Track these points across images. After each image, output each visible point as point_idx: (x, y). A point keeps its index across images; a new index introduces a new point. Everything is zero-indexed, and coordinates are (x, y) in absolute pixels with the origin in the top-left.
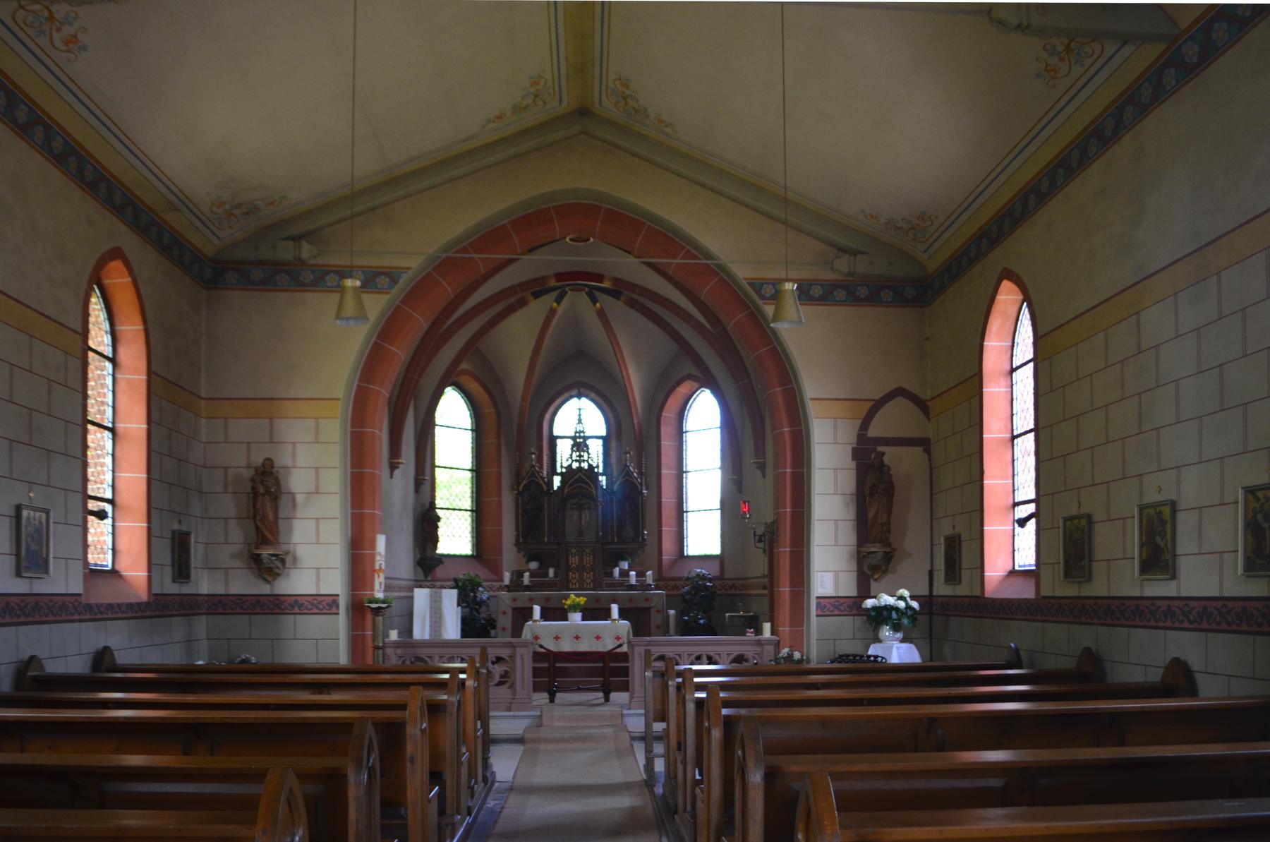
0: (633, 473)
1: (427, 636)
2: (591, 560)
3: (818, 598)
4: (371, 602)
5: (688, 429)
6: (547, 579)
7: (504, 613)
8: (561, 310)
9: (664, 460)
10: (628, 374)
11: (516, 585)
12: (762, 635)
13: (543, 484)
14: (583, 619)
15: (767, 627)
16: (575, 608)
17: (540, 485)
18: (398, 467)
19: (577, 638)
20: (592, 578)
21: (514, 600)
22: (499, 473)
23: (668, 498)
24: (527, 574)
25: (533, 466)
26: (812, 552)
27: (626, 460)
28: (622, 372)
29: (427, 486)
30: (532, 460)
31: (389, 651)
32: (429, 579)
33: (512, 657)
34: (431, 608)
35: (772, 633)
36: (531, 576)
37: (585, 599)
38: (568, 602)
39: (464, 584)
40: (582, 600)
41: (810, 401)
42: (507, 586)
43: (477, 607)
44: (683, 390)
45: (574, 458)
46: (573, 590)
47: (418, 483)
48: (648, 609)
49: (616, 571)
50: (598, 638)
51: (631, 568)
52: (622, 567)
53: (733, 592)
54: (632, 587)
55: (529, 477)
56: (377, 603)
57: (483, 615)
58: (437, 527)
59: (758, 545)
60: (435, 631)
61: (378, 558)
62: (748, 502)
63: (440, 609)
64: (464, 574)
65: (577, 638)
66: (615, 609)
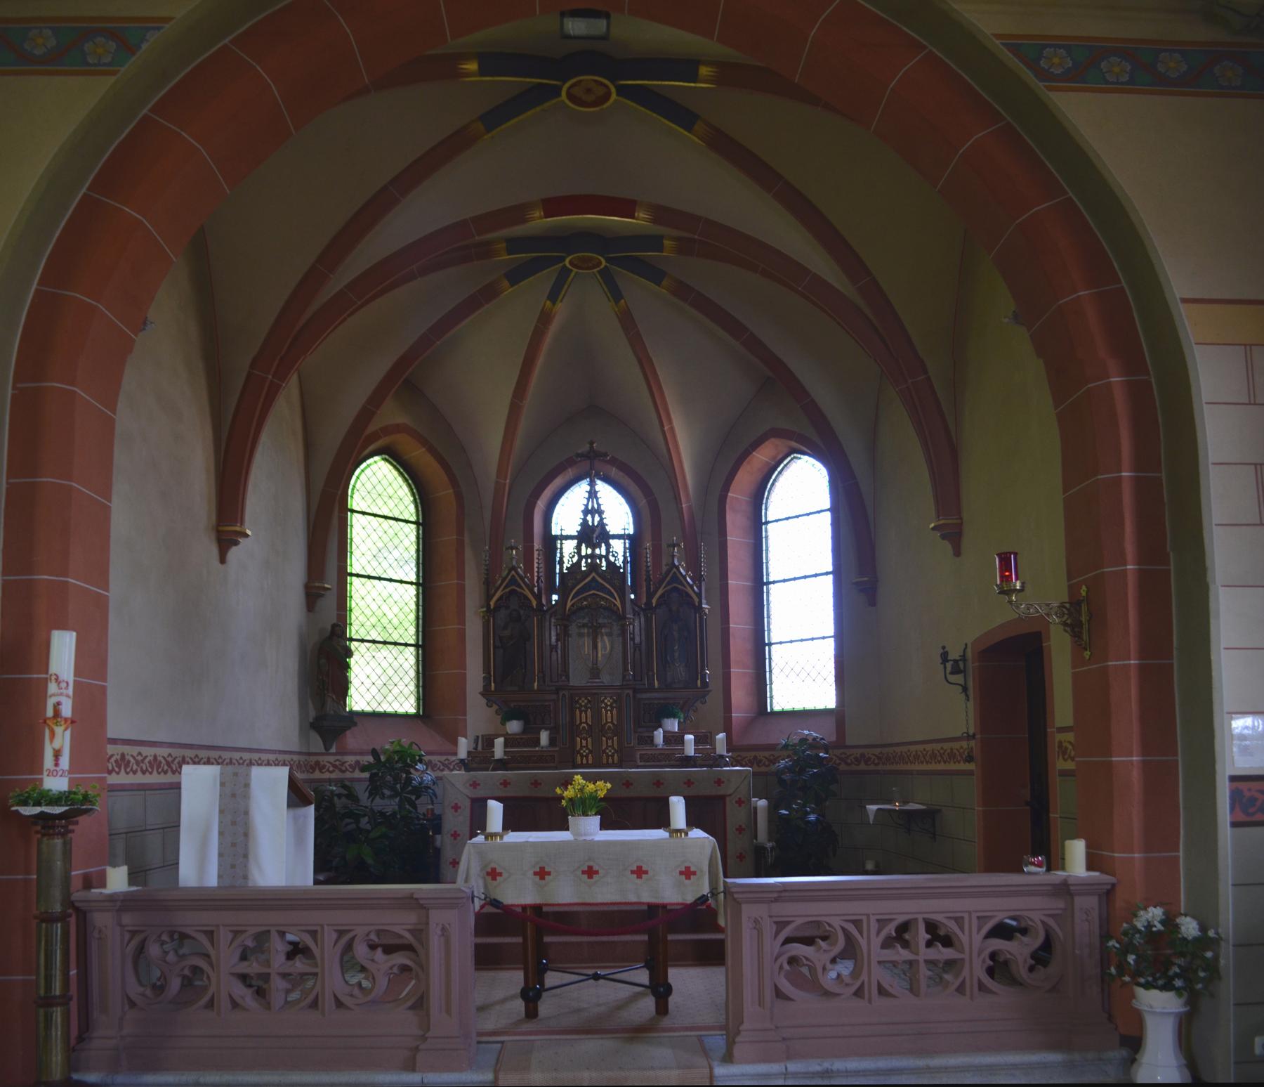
0: (684, 577)
1: (212, 880)
2: (615, 717)
3: (1234, 779)
4: (25, 803)
5: (769, 519)
6: (537, 749)
7: (456, 808)
8: (562, 310)
9: (732, 564)
10: (672, 429)
11: (480, 759)
12: (1063, 869)
13: (530, 596)
14: (604, 826)
15: (1077, 850)
16: (583, 805)
17: (526, 598)
18: (236, 543)
19: (590, 872)
20: (616, 747)
21: (475, 785)
22: (461, 590)
23: (739, 623)
24: (500, 742)
25: (514, 568)
26: (1214, 666)
27: (673, 556)
28: (662, 425)
29: (329, 602)
30: (512, 559)
31: (102, 920)
32: (333, 750)
33: (420, 932)
34: (221, 812)
35: (1090, 866)
36: (506, 744)
37: (609, 785)
38: (569, 793)
39: (389, 760)
40: (602, 788)
41: (1182, 306)
42: (462, 761)
43: (413, 798)
44: (761, 456)
45: (583, 553)
46: (582, 766)
47: (312, 596)
48: (722, 798)
49: (659, 735)
50: (639, 872)
51: (683, 730)
52: (669, 728)
53: (862, 767)
54: (687, 761)
55: (506, 586)
56: (38, 804)
57: (422, 810)
58: (347, 667)
59: (952, 678)
60: (233, 866)
61: (52, 688)
62: (1015, 554)
63: (247, 813)
64: (392, 743)
65: (590, 872)
66: (678, 806)
